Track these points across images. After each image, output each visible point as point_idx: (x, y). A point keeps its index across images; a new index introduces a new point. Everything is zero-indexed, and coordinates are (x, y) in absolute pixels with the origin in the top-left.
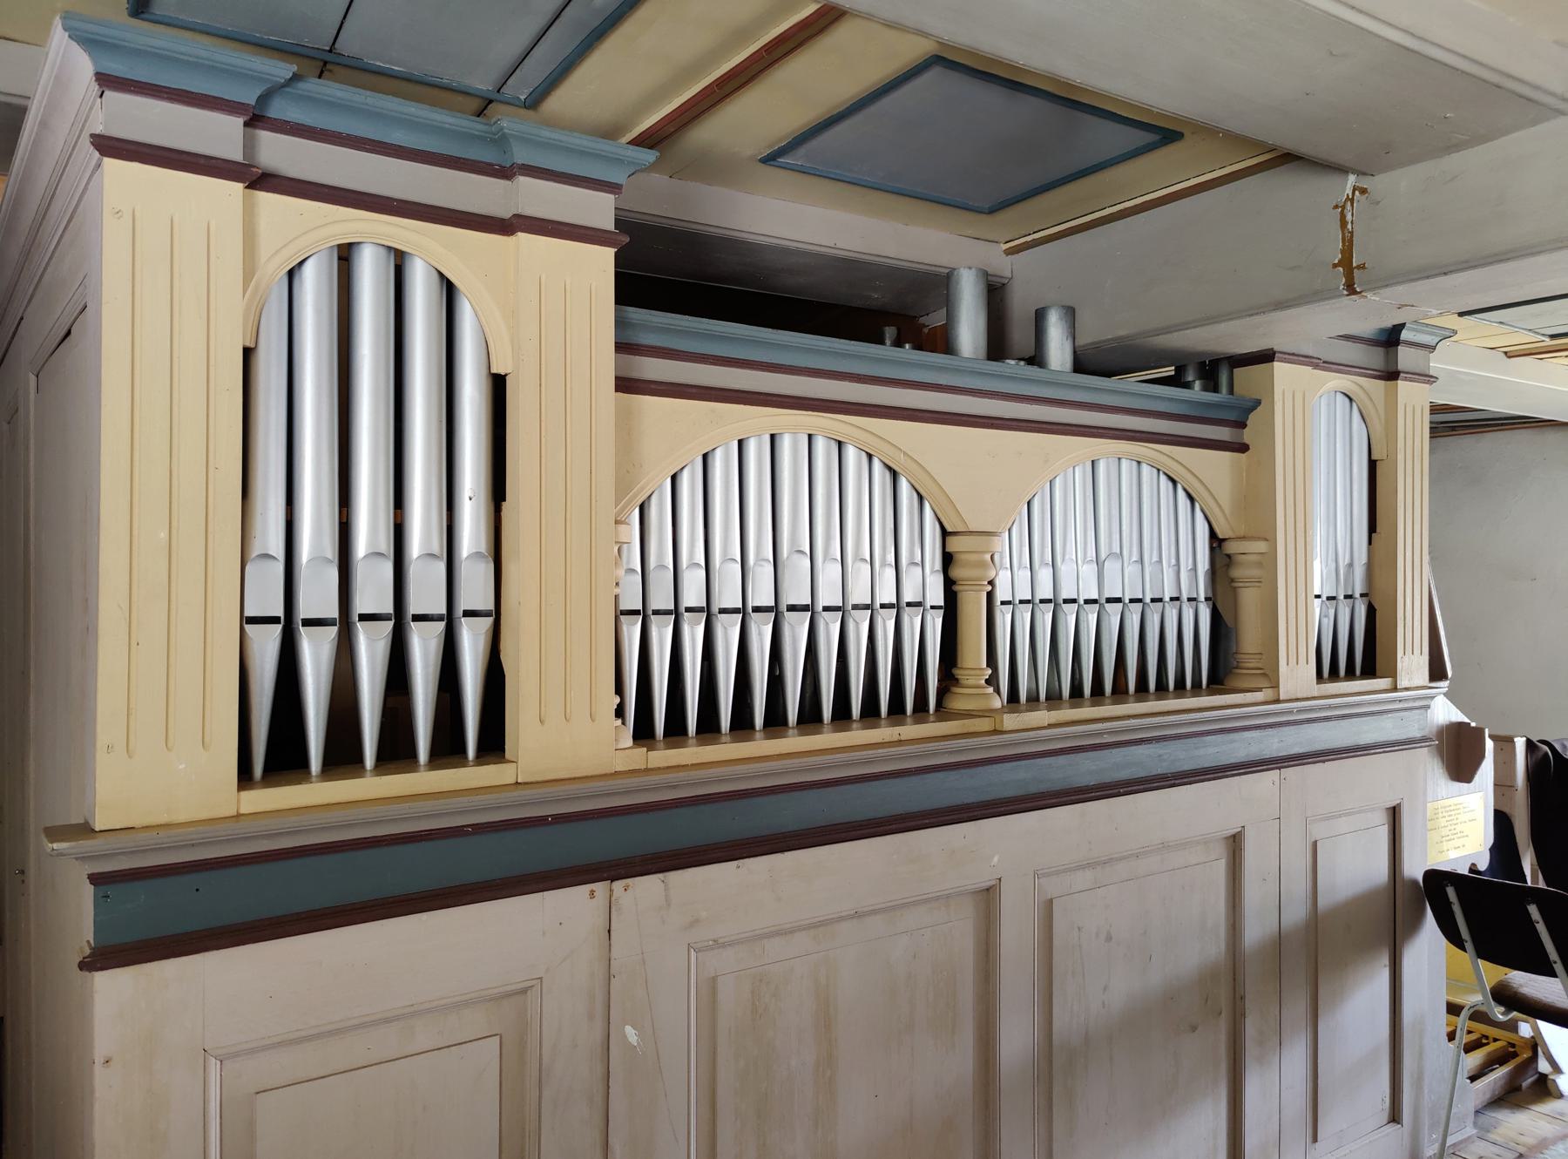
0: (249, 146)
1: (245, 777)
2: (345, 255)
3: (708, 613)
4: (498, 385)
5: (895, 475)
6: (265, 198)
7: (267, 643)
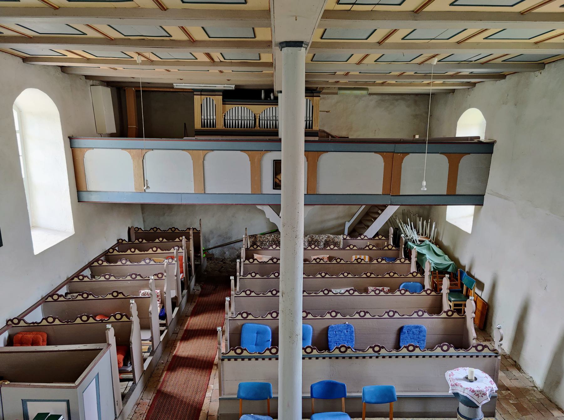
0: (201, 93)
1: (202, 127)
2: (207, 98)
3: (273, 120)
5: (247, 109)
6: (202, 96)
7: (203, 120)
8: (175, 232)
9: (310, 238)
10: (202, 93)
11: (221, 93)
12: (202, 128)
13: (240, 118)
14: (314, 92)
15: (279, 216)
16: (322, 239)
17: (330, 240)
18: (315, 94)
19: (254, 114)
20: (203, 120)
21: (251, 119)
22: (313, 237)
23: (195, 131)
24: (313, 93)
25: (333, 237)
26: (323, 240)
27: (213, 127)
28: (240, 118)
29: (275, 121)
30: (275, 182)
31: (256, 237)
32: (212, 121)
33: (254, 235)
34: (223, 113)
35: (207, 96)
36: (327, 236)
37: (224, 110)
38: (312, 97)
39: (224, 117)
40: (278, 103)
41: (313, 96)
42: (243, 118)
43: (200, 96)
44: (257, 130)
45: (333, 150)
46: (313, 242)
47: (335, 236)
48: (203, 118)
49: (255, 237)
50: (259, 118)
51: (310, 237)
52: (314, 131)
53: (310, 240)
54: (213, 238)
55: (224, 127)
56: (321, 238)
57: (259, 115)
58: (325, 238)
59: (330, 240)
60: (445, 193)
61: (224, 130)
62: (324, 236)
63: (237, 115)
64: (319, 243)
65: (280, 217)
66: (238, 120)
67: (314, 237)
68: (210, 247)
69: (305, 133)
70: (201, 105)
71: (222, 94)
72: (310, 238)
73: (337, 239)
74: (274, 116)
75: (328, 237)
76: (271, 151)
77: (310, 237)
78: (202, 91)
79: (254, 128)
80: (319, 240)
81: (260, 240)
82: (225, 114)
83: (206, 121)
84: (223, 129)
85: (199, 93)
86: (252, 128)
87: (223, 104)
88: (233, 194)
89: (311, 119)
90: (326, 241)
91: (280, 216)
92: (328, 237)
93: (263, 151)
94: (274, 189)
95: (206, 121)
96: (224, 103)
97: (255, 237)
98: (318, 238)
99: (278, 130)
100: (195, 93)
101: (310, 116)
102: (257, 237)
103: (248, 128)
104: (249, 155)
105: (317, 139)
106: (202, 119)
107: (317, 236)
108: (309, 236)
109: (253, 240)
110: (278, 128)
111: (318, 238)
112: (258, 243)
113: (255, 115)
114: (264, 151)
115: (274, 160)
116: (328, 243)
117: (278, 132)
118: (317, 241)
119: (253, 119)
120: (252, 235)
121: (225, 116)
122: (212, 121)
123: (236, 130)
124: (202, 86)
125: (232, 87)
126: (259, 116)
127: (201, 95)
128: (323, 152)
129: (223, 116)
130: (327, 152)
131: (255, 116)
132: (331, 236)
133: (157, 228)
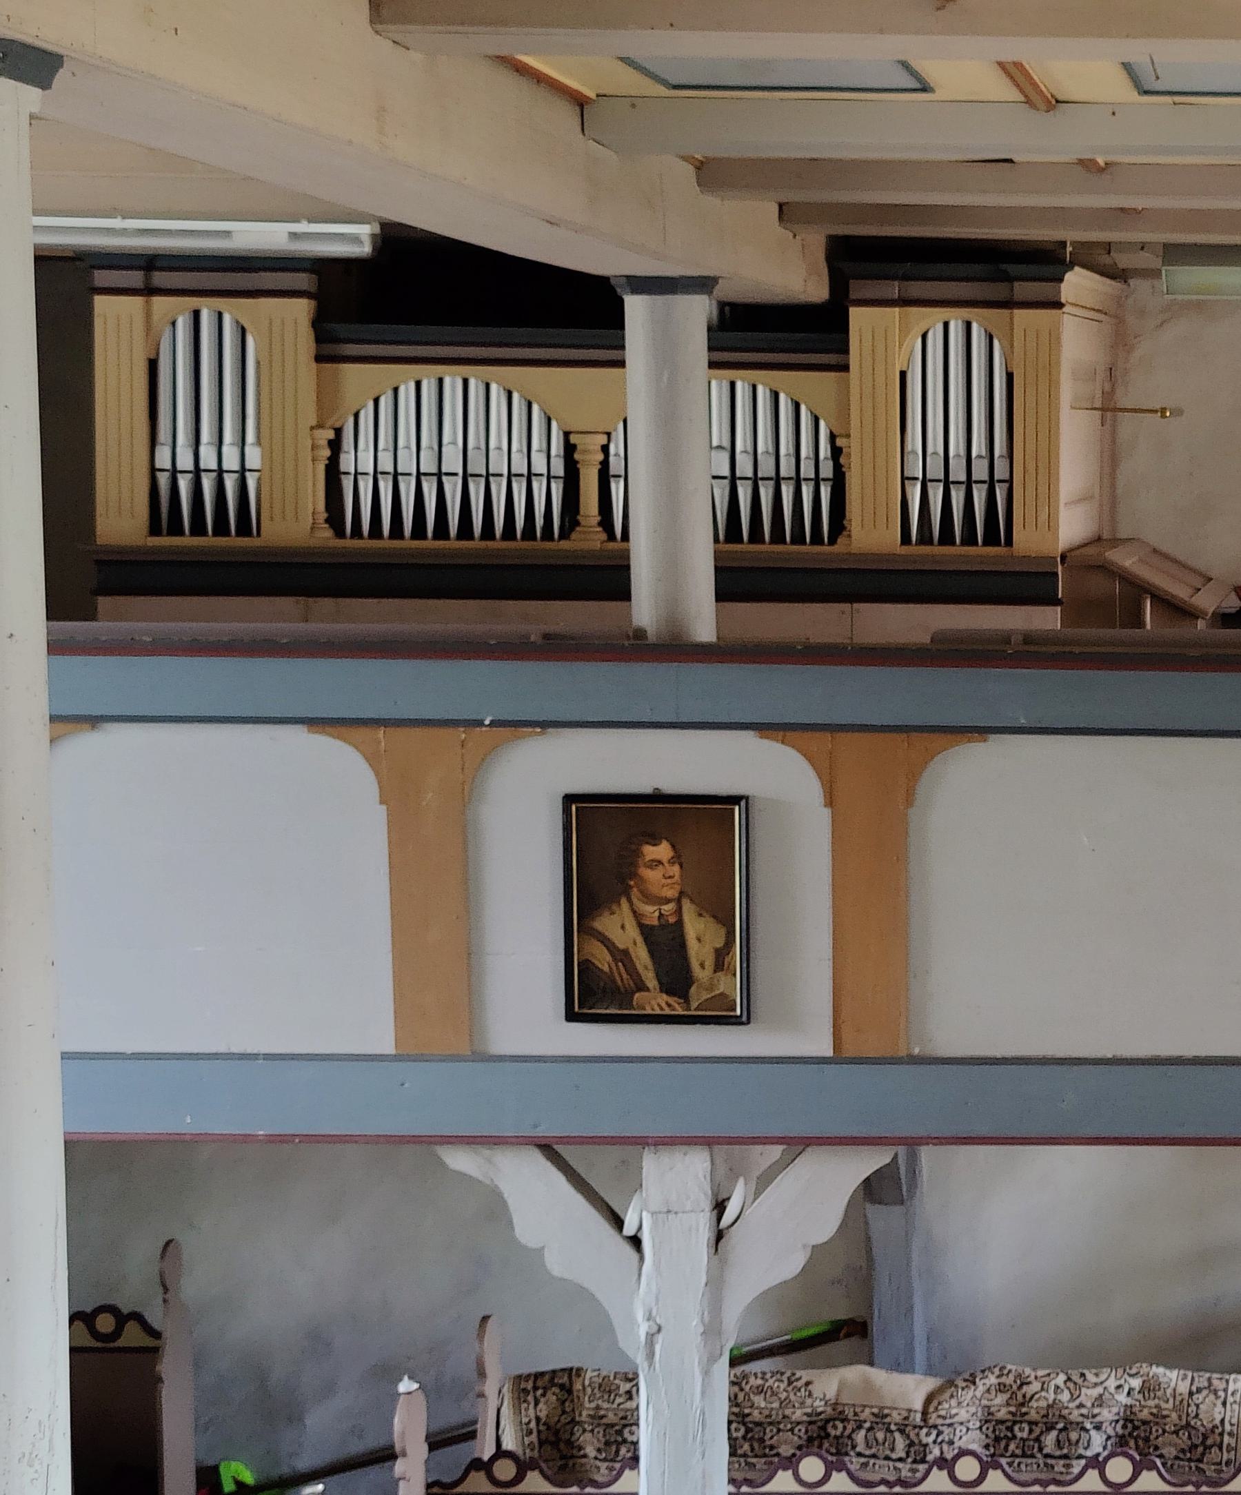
0: (147, 279)
1: (155, 529)
2: (196, 315)
4: (1010, 377)
8: (121, 1343)
9: (1001, 1399)
10: (161, 279)
11: (302, 280)
12: (905, 550)
13: (452, 462)
14: (1012, 269)
15: (618, 1222)
16: (1100, 1401)
17: (1159, 1417)
18: (1022, 290)
19: (567, 435)
20: (163, 480)
21: (539, 465)
22: (1029, 1390)
23: (98, 562)
24: (1009, 279)
25: (1183, 1388)
26: (1107, 1415)
27: (992, 537)
28: (452, 462)
29: (390, 478)
30: (586, 966)
31: (570, 1392)
32: (230, 483)
33: (554, 1372)
34: (320, 426)
35: (194, 302)
36: (1136, 1383)
37: (327, 399)
38: (1006, 312)
39: (327, 453)
40: (623, 347)
41: (1008, 304)
42: (477, 466)
43: (138, 301)
44: (591, 553)
45: (1023, 721)
46: (1022, 1432)
47: (1202, 1380)
48: (163, 458)
49: (562, 1387)
50: (605, 464)
51: (1002, 1388)
52: (1026, 558)
53: (1002, 1414)
54: (328, 1390)
55: (326, 533)
56: (1091, 1393)
57: (603, 440)
58: (1122, 1398)
59: (1159, 1417)
60: (388, 1048)
61: (333, 552)
62: (1112, 1384)
63: (978, 447)
64: (1074, 1436)
65: (636, 1241)
66: (439, 475)
67: (1036, 1386)
68: (304, 1463)
69: (720, 571)
70: (153, 365)
71: (313, 289)
72: (1001, 1399)
73: (1219, 1408)
74: (720, 447)
75: (1149, 1388)
76: (545, 725)
77: (1002, 1388)
78: (150, 262)
79: (564, 535)
80: (1075, 1416)
81: (597, 1418)
82: (339, 432)
83: (184, 484)
84: (313, 543)
85: (135, 278)
86: (817, 538)
87: (319, 359)
88: (255, 1056)
89: (1001, 472)
90: (1129, 1419)
91: (629, 1229)
92: (1149, 1388)
93: (480, 723)
94: (571, 1016)
95: (184, 484)
96: (329, 349)
97: (562, 1387)
98: (1065, 1397)
99: (626, 555)
100: (102, 278)
101: (997, 453)
102: (578, 1386)
103: (424, 537)
104: (372, 759)
105: (1047, 619)
106: (153, 470)
107: (1061, 1379)
108: (992, 1380)
109: (543, 1410)
110: (626, 536)
111: (1065, 1397)
112: (588, 1436)
113: (573, 439)
114: (493, 724)
115: (569, 799)
116: (1147, 1440)
117: (628, 567)
118: (1052, 1419)
119: (558, 468)
120: (538, 1376)
121: (335, 446)
122: (230, 483)
123: (421, 553)
124: (124, 232)
125: (355, 239)
126: (605, 449)
127: (150, 291)
128: (70, 726)
129: (314, 447)
130: (983, 732)
131: (570, 449)
132: (1173, 1379)
133: (125, 1311)
